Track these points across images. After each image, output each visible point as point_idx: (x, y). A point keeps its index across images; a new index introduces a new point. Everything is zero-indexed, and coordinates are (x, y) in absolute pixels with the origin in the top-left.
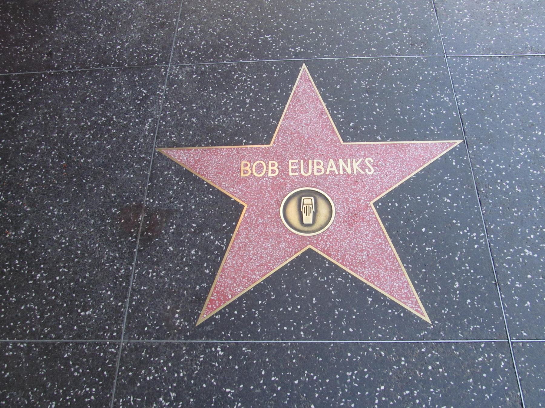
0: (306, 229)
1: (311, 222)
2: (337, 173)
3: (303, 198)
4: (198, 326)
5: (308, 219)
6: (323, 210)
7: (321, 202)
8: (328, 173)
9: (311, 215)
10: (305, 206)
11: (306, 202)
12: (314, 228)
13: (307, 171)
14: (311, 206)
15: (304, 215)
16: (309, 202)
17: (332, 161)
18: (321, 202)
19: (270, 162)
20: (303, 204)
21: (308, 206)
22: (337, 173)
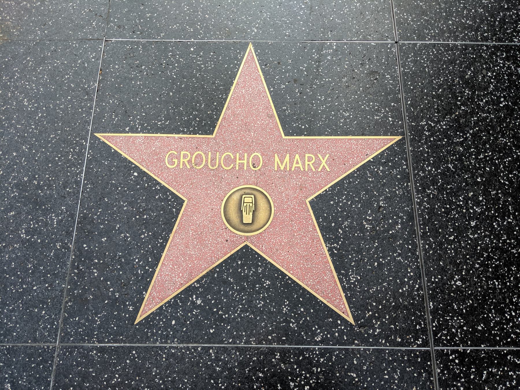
0: (246, 228)
1: (251, 222)
2: (302, 170)
3: (244, 196)
4: (140, 323)
5: (247, 218)
6: (262, 204)
7: (259, 196)
8: (293, 169)
9: (251, 214)
10: (245, 204)
11: (246, 200)
12: (242, 192)
14: (251, 204)
15: (244, 213)
16: (250, 200)
17: (297, 156)
18: (259, 196)
20: (244, 203)
21: (248, 204)
22: (302, 170)
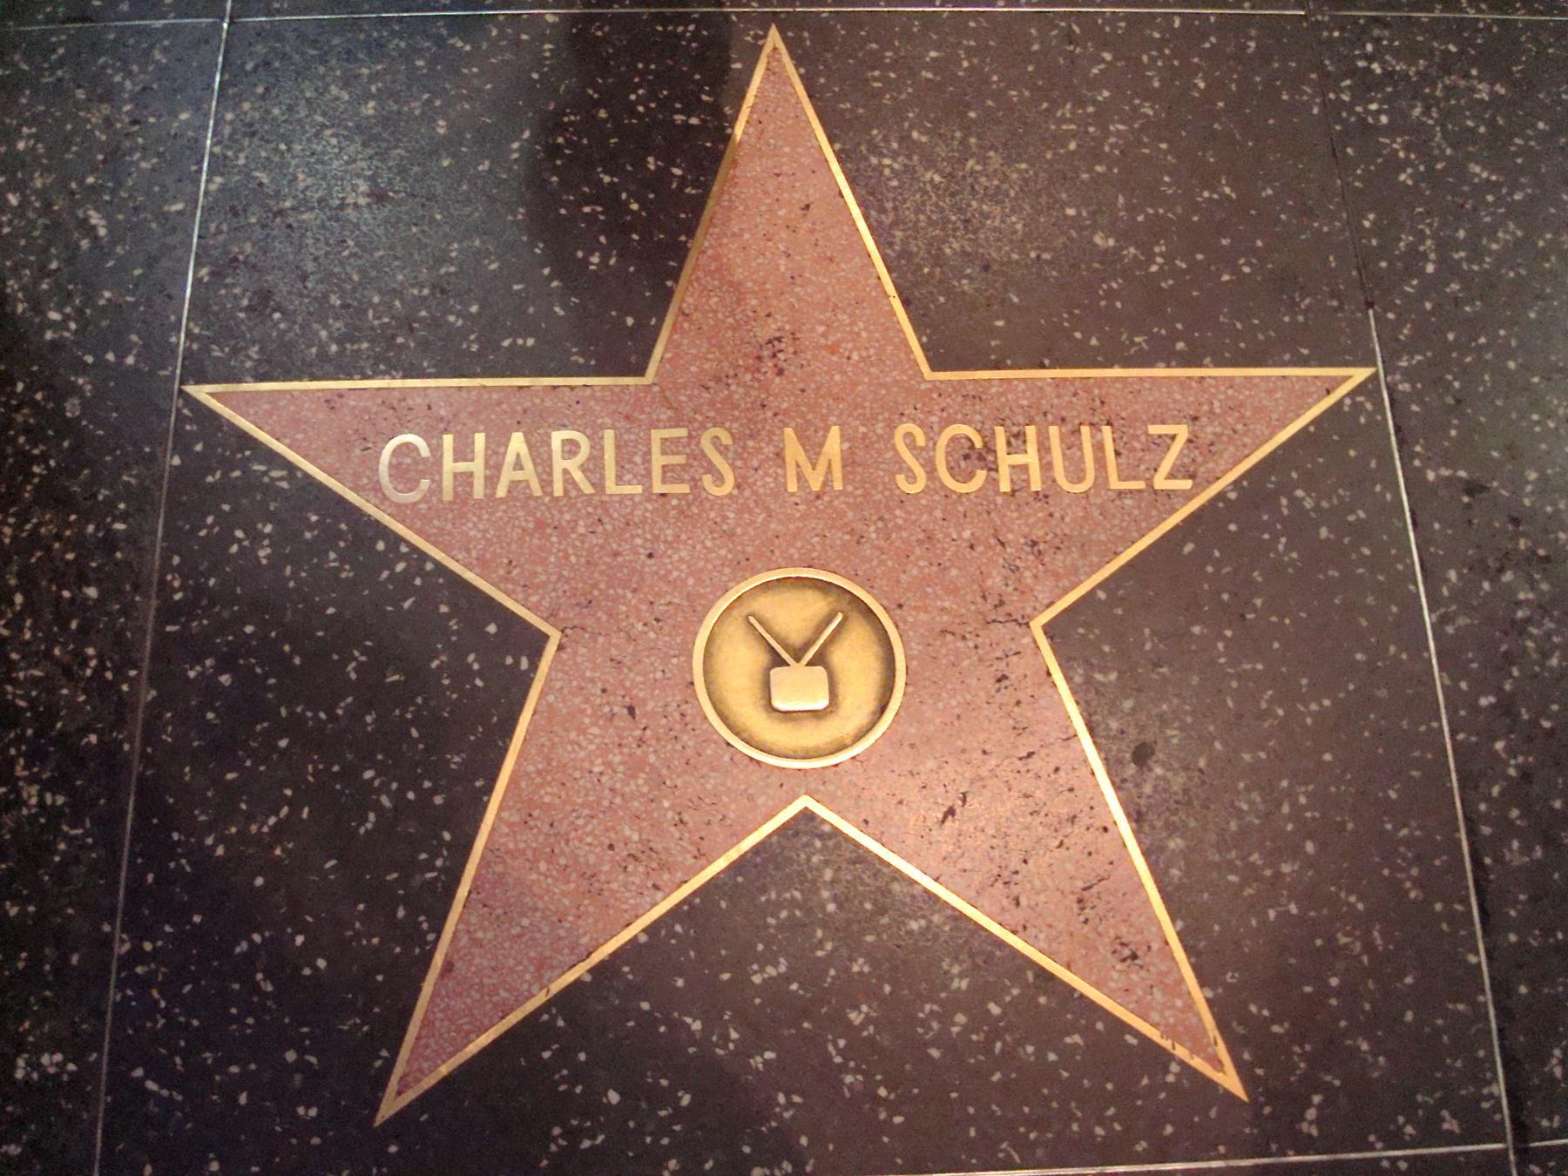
8: (501, 492)
13: (1077, 475)
17: (517, 443)
19: (557, 438)
